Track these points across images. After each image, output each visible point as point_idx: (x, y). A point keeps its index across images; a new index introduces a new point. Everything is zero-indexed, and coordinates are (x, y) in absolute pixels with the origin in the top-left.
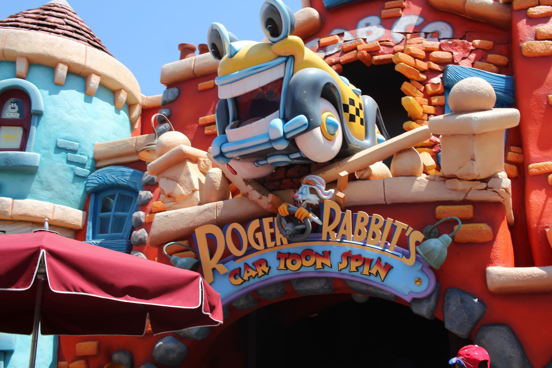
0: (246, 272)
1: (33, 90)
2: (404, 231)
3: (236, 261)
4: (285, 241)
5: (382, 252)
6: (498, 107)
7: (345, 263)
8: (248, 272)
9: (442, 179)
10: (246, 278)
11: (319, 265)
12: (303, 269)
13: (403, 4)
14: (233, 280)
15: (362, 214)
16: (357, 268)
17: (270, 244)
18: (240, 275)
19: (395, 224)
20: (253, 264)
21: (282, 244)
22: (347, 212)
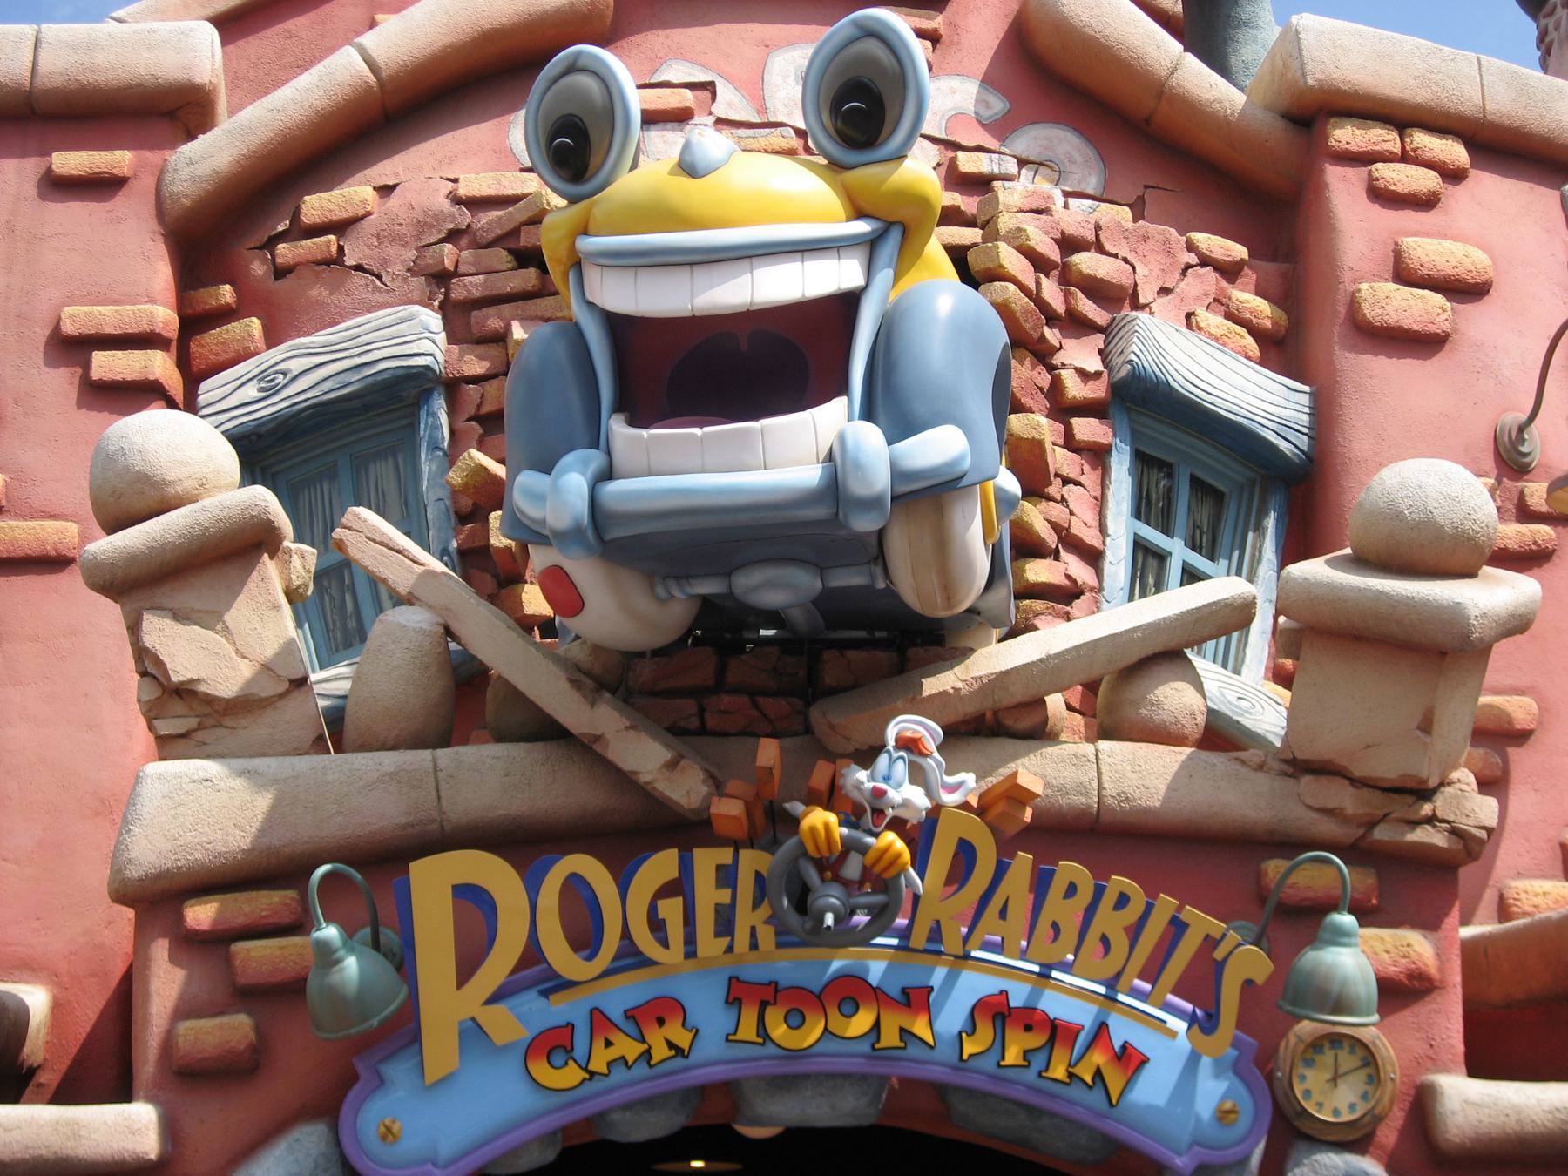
0: (599, 1044)
1: (397, 330)
2: (1210, 943)
3: (550, 997)
4: (767, 936)
5: (1107, 1001)
6: (227, 437)
7: (985, 1034)
8: (608, 1044)
9: (1290, 770)
10: (598, 1064)
11: (890, 1038)
12: (831, 1046)
13: (1246, 250)
14: (541, 1071)
15: (1069, 870)
16: (1026, 1054)
17: (710, 944)
18: (568, 1050)
19: (1182, 916)
20: (629, 1015)
21: (754, 946)
22: (1159, 899)
